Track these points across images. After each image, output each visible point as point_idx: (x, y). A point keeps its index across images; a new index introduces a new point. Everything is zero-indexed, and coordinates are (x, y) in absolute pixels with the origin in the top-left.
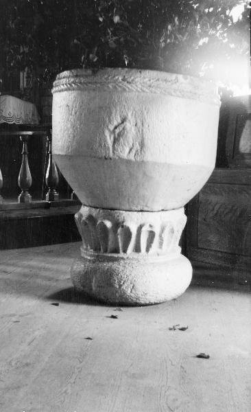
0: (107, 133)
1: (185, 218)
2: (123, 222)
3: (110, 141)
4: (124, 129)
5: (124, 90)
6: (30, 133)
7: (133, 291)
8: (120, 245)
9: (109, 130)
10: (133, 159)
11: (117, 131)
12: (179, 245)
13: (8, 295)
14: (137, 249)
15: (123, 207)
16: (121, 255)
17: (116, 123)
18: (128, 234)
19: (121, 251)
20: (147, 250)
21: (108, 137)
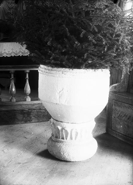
0: (57, 94)
1: (110, 75)
2: (65, 128)
3: (58, 98)
4: (63, 92)
5: (63, 77)
6: (19, 10)
7: (68, 156)
8: (65, 137)
9: (57, 93)
10: (67, 105)
11: (60, 93)
12: (99, 120)
13: (21, 55)
14: (71, 138)
15: (65, 122)
16: (65, 140)
17: (60, 90)
18: (66, 131)
19: (65, 139)
20: (75, 139)
21: (57, 95)
